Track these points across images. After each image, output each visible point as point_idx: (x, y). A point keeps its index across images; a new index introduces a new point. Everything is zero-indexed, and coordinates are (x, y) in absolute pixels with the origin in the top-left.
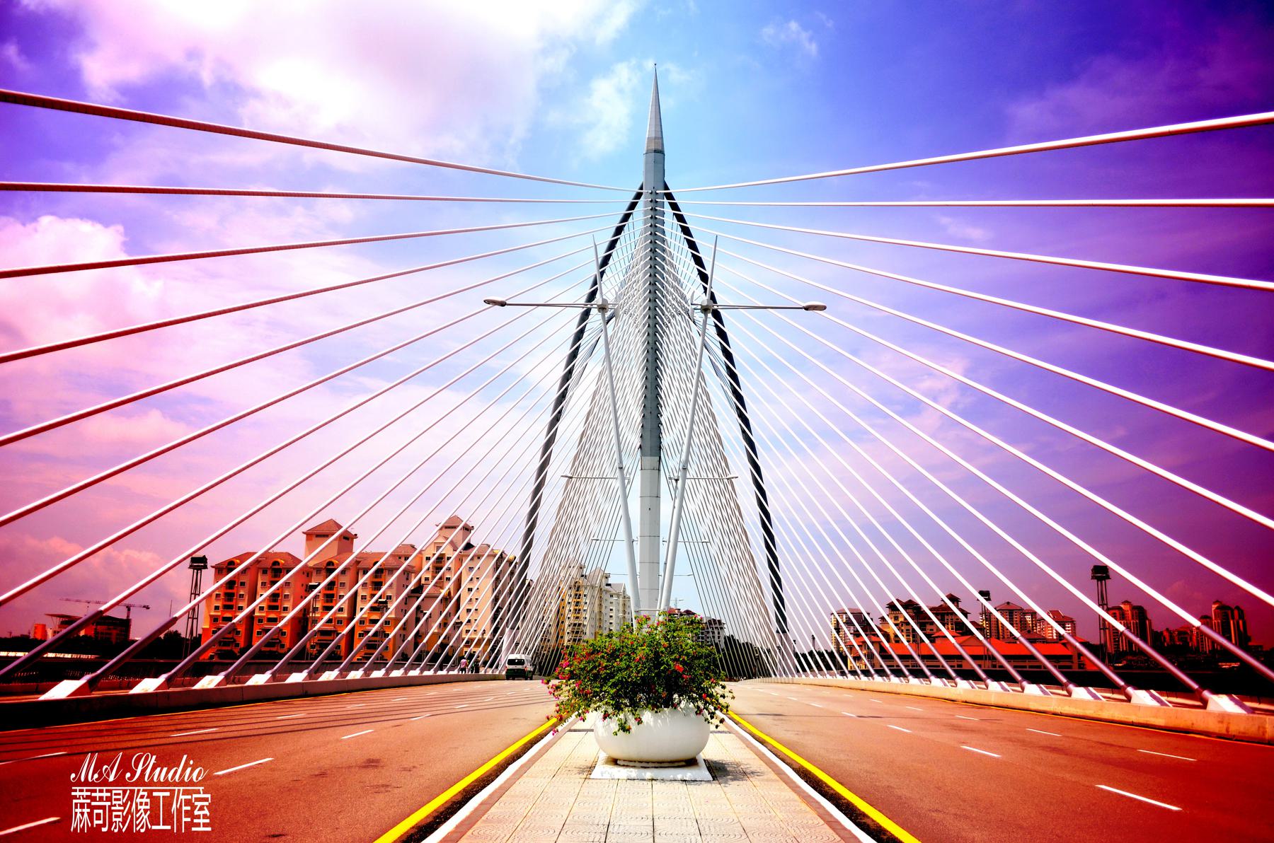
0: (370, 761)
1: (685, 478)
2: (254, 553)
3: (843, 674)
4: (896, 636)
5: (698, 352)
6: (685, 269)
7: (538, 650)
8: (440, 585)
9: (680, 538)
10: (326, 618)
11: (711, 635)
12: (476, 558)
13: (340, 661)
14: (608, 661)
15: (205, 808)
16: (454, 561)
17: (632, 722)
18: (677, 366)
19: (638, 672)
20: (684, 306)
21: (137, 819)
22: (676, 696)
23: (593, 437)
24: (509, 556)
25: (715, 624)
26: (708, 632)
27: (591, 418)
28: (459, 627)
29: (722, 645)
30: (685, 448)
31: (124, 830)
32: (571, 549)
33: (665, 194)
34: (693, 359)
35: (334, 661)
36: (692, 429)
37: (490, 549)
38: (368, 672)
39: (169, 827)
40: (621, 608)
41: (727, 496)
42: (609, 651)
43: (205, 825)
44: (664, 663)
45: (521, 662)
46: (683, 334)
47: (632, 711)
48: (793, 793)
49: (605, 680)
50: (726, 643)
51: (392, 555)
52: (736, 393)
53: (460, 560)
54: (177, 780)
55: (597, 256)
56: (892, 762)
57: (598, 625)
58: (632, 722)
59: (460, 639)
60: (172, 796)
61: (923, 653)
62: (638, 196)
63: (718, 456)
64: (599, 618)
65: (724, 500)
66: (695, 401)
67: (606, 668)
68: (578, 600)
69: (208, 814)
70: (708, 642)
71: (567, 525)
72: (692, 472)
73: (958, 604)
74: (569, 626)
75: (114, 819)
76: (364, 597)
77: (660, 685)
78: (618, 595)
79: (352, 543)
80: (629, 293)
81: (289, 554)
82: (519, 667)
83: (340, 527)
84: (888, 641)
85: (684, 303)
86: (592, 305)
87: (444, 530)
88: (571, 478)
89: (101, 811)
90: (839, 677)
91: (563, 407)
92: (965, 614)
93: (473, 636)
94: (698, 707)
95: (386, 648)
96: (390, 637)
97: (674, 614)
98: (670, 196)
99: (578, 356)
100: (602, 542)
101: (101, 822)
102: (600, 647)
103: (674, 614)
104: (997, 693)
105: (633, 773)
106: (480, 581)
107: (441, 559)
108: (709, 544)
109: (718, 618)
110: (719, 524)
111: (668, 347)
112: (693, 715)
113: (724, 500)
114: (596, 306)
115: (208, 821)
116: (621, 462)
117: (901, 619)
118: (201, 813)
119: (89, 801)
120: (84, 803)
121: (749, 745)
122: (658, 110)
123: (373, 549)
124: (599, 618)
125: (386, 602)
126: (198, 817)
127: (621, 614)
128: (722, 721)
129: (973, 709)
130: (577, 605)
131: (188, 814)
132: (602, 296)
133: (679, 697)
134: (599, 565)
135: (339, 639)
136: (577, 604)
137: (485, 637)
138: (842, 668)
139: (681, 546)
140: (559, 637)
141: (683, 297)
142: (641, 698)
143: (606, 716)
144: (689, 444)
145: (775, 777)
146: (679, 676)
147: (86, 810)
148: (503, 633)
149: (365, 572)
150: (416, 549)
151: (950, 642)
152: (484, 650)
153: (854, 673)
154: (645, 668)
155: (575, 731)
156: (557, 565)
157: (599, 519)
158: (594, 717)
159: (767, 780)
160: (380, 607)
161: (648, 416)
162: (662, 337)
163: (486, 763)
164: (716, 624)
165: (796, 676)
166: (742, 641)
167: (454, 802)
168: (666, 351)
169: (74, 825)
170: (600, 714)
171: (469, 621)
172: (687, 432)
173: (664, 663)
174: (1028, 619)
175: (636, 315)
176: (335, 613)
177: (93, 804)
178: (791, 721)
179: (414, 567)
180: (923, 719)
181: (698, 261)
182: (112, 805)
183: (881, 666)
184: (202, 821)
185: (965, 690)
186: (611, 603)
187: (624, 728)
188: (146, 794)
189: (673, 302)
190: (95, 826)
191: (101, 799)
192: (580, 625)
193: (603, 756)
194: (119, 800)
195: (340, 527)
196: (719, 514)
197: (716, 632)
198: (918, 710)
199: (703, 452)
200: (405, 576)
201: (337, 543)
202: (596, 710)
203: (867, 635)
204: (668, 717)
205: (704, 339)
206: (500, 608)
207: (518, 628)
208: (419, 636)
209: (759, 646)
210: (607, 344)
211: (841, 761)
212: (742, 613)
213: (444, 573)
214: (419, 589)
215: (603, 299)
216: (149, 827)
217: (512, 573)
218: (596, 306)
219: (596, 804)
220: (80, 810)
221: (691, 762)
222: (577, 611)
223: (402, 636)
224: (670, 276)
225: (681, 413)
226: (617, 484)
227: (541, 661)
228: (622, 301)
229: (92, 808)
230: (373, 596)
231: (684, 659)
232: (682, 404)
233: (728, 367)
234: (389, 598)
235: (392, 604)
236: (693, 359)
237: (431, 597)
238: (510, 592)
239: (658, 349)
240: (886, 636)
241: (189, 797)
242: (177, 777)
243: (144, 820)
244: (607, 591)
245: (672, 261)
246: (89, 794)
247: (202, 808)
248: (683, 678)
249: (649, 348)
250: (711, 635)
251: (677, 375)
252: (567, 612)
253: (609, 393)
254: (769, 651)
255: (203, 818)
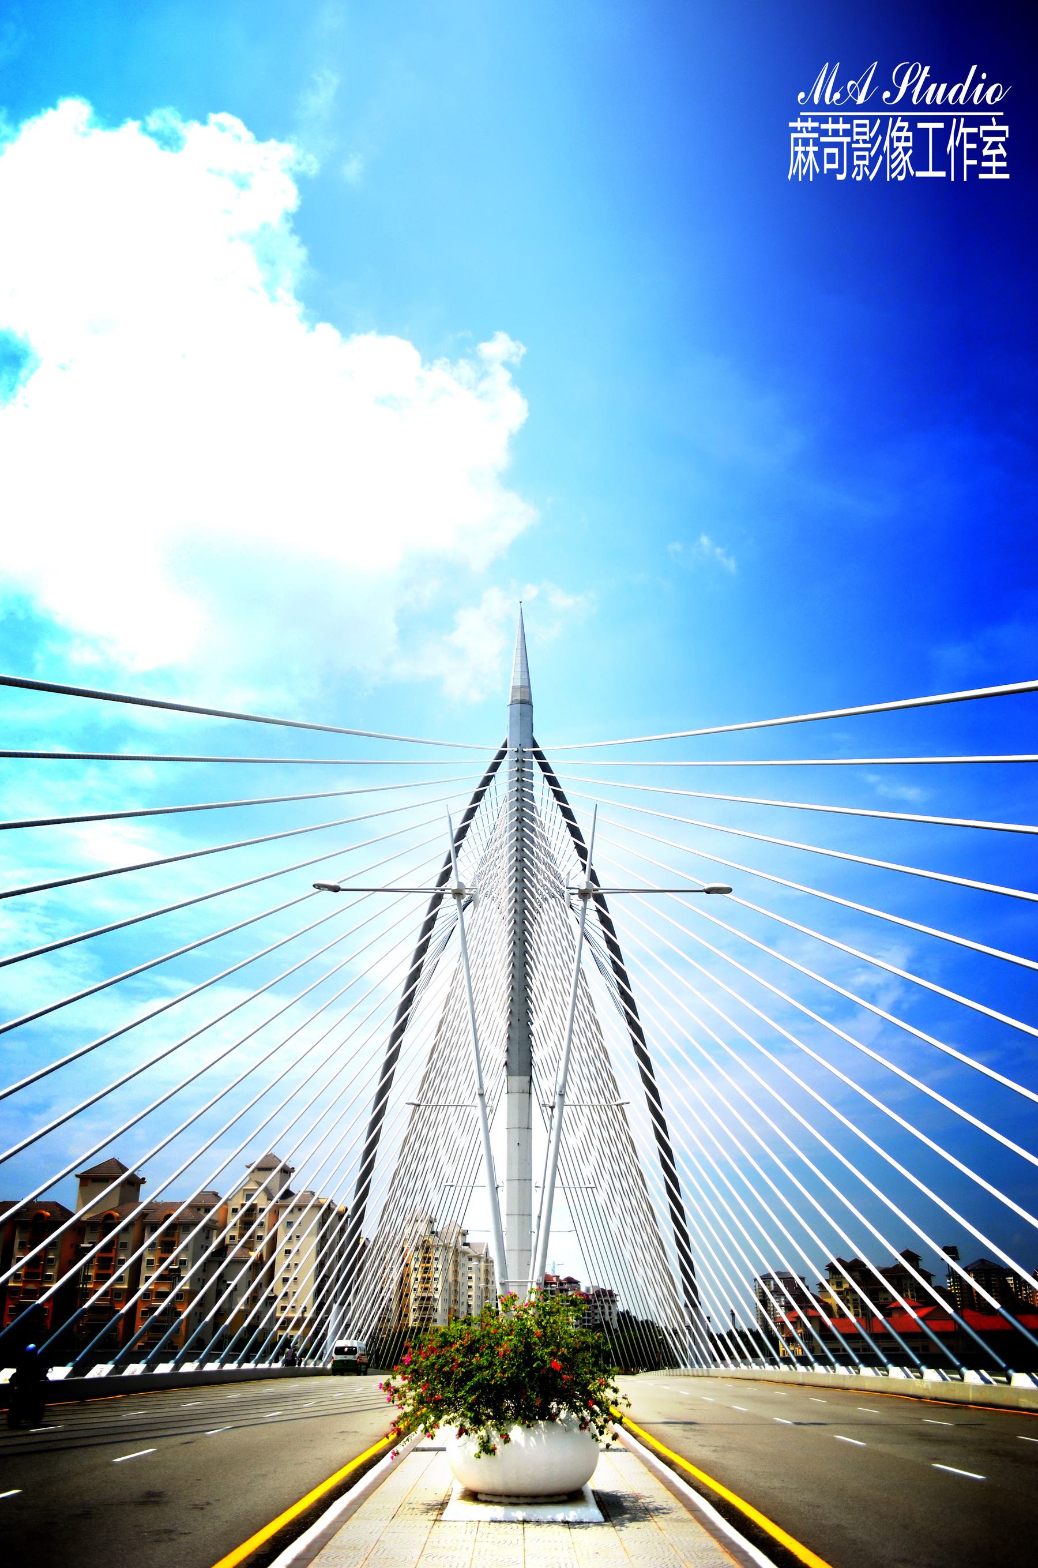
0: (150, 1495)
1: (562, 1105)
2: (15, 1203)
3: (773, 1362)
4: (840, 1308)
5: (577, 943)
6: (559, 843)
7: (375, 1334)
8: (249, 1246)
9: (558, 1183)
10: (102, 1290)
11: (600, 1310)
12: (296, 1210)
13: (116, 1350)
14: (464, 1356)
15: (1000, 145)
16: (268, 1215)
17: (496, 1440)
18: (551, 961)
19: (504, 1372)
20: (558, 887)
21: (892, 162)
22: (554, 1404)
23: (447, 1052)
24: (339, 1207)
25: (605, 1295)
26: (596, 1307)
27: (443, 1028)
28: (272, 1304)
29: (615, 1325)
30: (562, 1064)
31: (871, 178)
32: (418, 1198)
33: (534, 752)
34: (571, 952)
35: (108, 1350)
36: (570, 1040)
37: (315, 1198)
38: (151, 1366)
39: (943, 174)
40: (483, 1276)
41: (617, 1127)
42: (467, 1342)
43: (999, 170)
44: (537, 1359)
45: (352, 1351)
46: (558, 922)
47: (496, 1425)
48: (711, 1538)
49: (461, 1382)
50: (619, 1321)
51: (190, 1206)
52: (624, 994)
53: (276, 1212)
54: (961, 102)
55: (451, 828)
56: (841, 1489)
57: (452, 1298)
58: (496, 1440)
59: (274, 1319)
60: (948, 126)
61: (876, 1331)
62: (502, 755)
63: (605, 1075)
64: (454, 1290)
65: (612, 1133)
66: (574, 1004)
67: (462, 1364)
68: (427, 1265)
69: (1005, 155)
70: (596, 1320)
71: (414, 1166)
72: (571, 1097)
73: (918, 1263)
74: (416, 1300)
75: (856, 162)
76: (150, 1262)
77: (533, 1389)
78: (479, 1258)
79: (138, 1190)
80: (491, 872)
81: (57, 1205)
82: (350, 1357)
83: (125, 1170)
84: (830, 1315)
85: (559, 883)
86: (444, 890)
87: (256, 1172)
88: (419, 1105)
89: (835, 151)
90: (769, 1368)
91: (409, 1014)
92: (927, 1277)
93: (291, 1315)
94: (583, 1419)
95: (177, 1330)
96: (183, 1317)
97: (551, 1284)
98: (539, 755)
99: (429, 950)
100: (458, 1189)
101: (835, 166)
102: (453, 1337)
103: (551, 1284)
104: (976, 1387)
105: (498, 1511)
106: (302, 1239)
107: (252, 1211)
108: (594, 1190)
109: (608, 1288)
110: (607, 1164)
111: (539, 937)
112: (576, 1430)
113: (612, 1133)
114: (450, 891)
115: (1004, 164)
116: (481, 1086)
117: (845, 1286)
118: (994, 152)
119: (816, 135)
120: (809, 139)
121: (652, 1469)
122: (524, 655)
123: (165, 1199)
124: (454, 1290)
125: (178, 1270)
126: (989, 158)
127: (482, 1285)
128: (615, 1437)
129: (946, 1410)
130: (425, 1272)
131: (972, 154)
132: (457, 876)
133: (558, 1405)
134: (454, 1219)
135: (116, 1320)
136: (426, 1270)
137: (305, 1315)
138: (771, 1355)
139: (558, 1193)
140: (403, 1315)
141: (557, 876)
142: (508, 1407)
143: (462, 1431)
144: (568, 1060)
145: (688, 1515)
146: (557, 1375)
147: (812, 149)
148: (329, 1311)
149: (154, 1229)
150: (220, 1199)
151: (910, 1316)
152: (305, 1334)
153: (787, 1361)
154: (513, 1365)
155: (423, 1450)
156: (400, 1220)
157: (453, 1159)
158: (446, 1432)
159: (678, 1520)
160: (171, 1277)
161: (515, 1023)
162: (532, 926)
163: (304, 1496)
164: (606, 1296)
165: (713, 1366)
166: (640, 1319)
167: (260, 1555)
168: (537, 943)
169: (792, 171)
170: (454, 1428)
171: (286, 1294)
172: (565, 1044)
173: (537, 1359)
174: (1010, 1282)
175: (499, 898)
176: (112, 1285)
177: (823, 139)
178: (706, 1432)
179: (217, 1222)
180: (880, 1424)
181: (575, 832)
182: (852, 142)
183: (823, 1351)
184: (994, 164)
185: (934, 1384)
186: (470, 1268)
187: (487, 1448)
188: (906, 125)
189: (544, 882)
190: (825, 172)
191: (836, 133)
192: (429, 1298)
193: (458, 1490)
194: (864, 133)
195: (125, 1170)
196: (607, 1150)
197: (606, 1306)
198: (872, 1412)
199: (585, 1070)
200: (204, 1235)
201: (119, 1188)
202: (449, 1423)
203: (801, 1308)
204: (544, 1432)
205: (583, 928)
206: (326, 1277)
207: (349, 1304)
208: (221, 1315)
209: (662, 1325)
210: (464, 936)
211: (775, 1488)
212: (640, 1282)
213: (254, 1231)
214: (222, 1250)
215: (458, 882)
216: (912, 172)
217: (342, 1230)
218: (450, 891)
219: (449, 1559)
220: (803, 149)
221: (574, 1496)
222: (426, 1280)
223: (198, 1315)
224: (540, 851)
225: (557, 1020)
226: (477, 1112)
227: (379, 1349)
228: (483, 882)
229: (823, 146)
230: (162, 1261)
231: (563, 1353)
232: (558, 1010)
233: (614, 962)
234: (183, 1262)
235: (187, 1271)
236: (571, 952)
237: (238, 1262)
238: (340, 1255)
239: (527, 941)
240: (827, 1308)
241: (974, 130)
242: (961, 99)
243: (903, 163)
244: (464, 1253)
245: (543, 832)
246: (816, 125)
247: (994, 146)
248: (562, 1379)
249: (516, 939)
250: (600, 1310)
251: (551, 973)
252: (412, 1281)
253: (466, 996)
254: (675, 1332)
255: (992, 168)
